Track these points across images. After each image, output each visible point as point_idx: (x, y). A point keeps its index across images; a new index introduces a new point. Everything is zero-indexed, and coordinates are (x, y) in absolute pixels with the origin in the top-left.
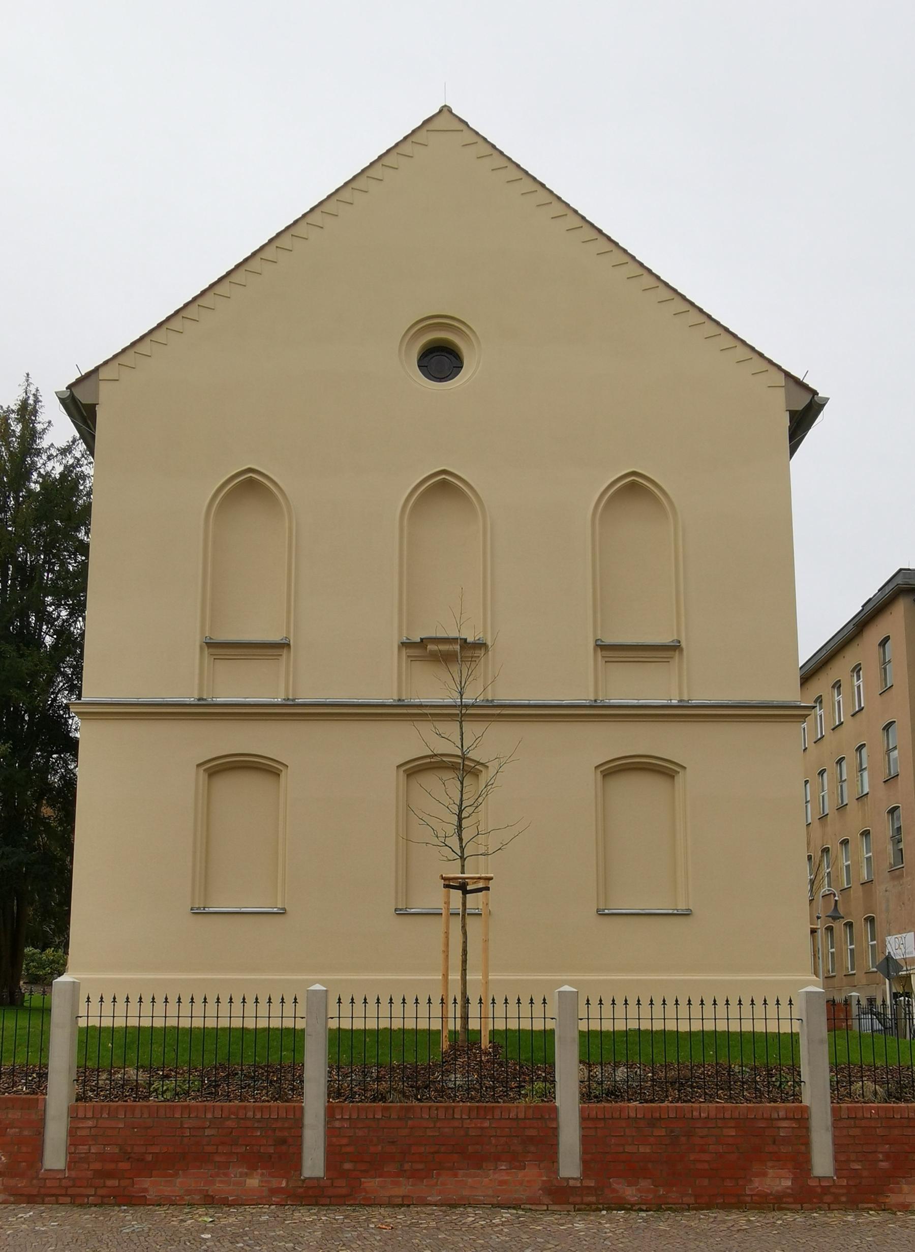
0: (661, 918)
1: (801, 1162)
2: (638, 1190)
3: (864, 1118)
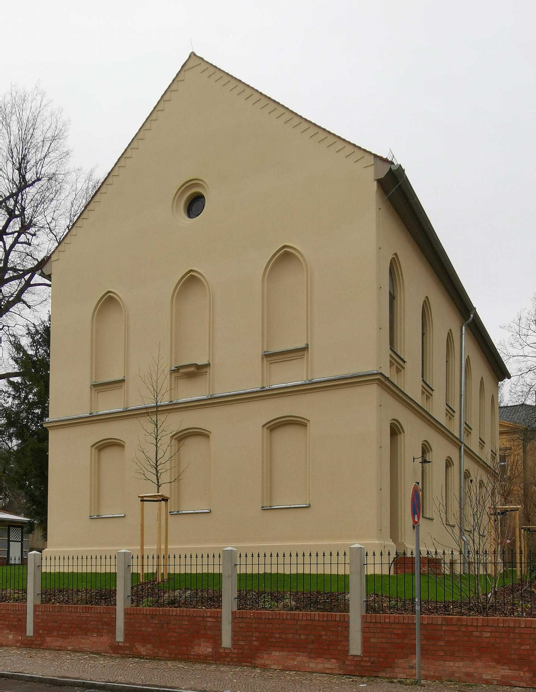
0: (285, 510)
1: (217, 639)
2: (146, 649)
3: (247, 618)
